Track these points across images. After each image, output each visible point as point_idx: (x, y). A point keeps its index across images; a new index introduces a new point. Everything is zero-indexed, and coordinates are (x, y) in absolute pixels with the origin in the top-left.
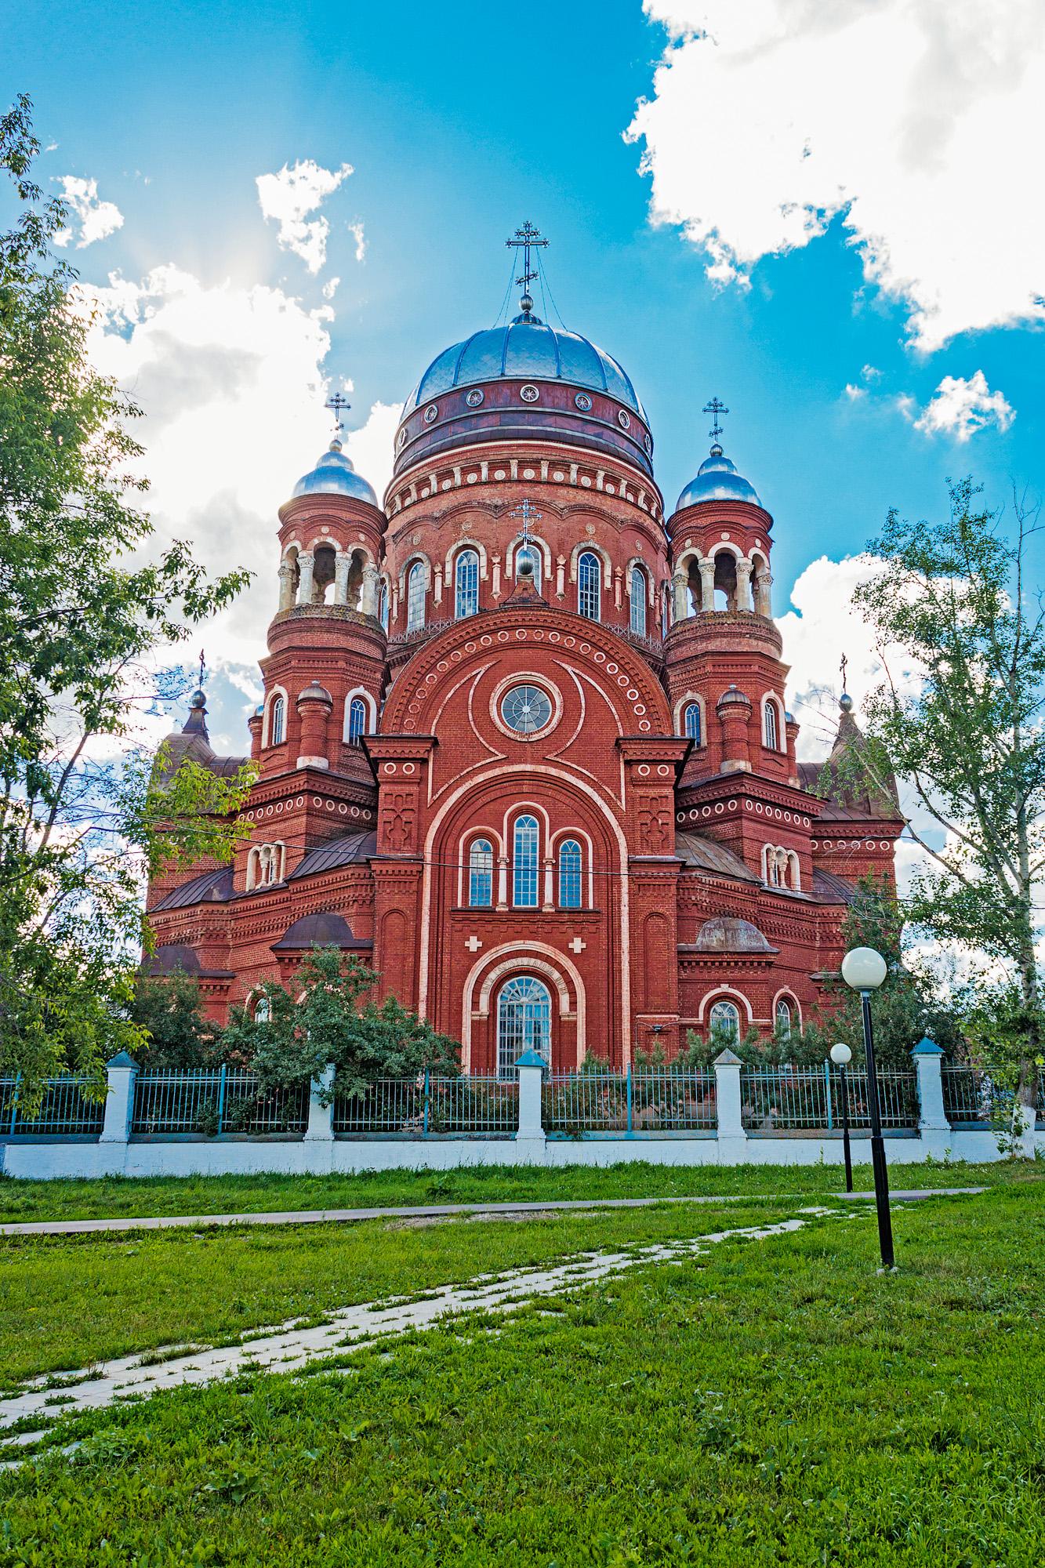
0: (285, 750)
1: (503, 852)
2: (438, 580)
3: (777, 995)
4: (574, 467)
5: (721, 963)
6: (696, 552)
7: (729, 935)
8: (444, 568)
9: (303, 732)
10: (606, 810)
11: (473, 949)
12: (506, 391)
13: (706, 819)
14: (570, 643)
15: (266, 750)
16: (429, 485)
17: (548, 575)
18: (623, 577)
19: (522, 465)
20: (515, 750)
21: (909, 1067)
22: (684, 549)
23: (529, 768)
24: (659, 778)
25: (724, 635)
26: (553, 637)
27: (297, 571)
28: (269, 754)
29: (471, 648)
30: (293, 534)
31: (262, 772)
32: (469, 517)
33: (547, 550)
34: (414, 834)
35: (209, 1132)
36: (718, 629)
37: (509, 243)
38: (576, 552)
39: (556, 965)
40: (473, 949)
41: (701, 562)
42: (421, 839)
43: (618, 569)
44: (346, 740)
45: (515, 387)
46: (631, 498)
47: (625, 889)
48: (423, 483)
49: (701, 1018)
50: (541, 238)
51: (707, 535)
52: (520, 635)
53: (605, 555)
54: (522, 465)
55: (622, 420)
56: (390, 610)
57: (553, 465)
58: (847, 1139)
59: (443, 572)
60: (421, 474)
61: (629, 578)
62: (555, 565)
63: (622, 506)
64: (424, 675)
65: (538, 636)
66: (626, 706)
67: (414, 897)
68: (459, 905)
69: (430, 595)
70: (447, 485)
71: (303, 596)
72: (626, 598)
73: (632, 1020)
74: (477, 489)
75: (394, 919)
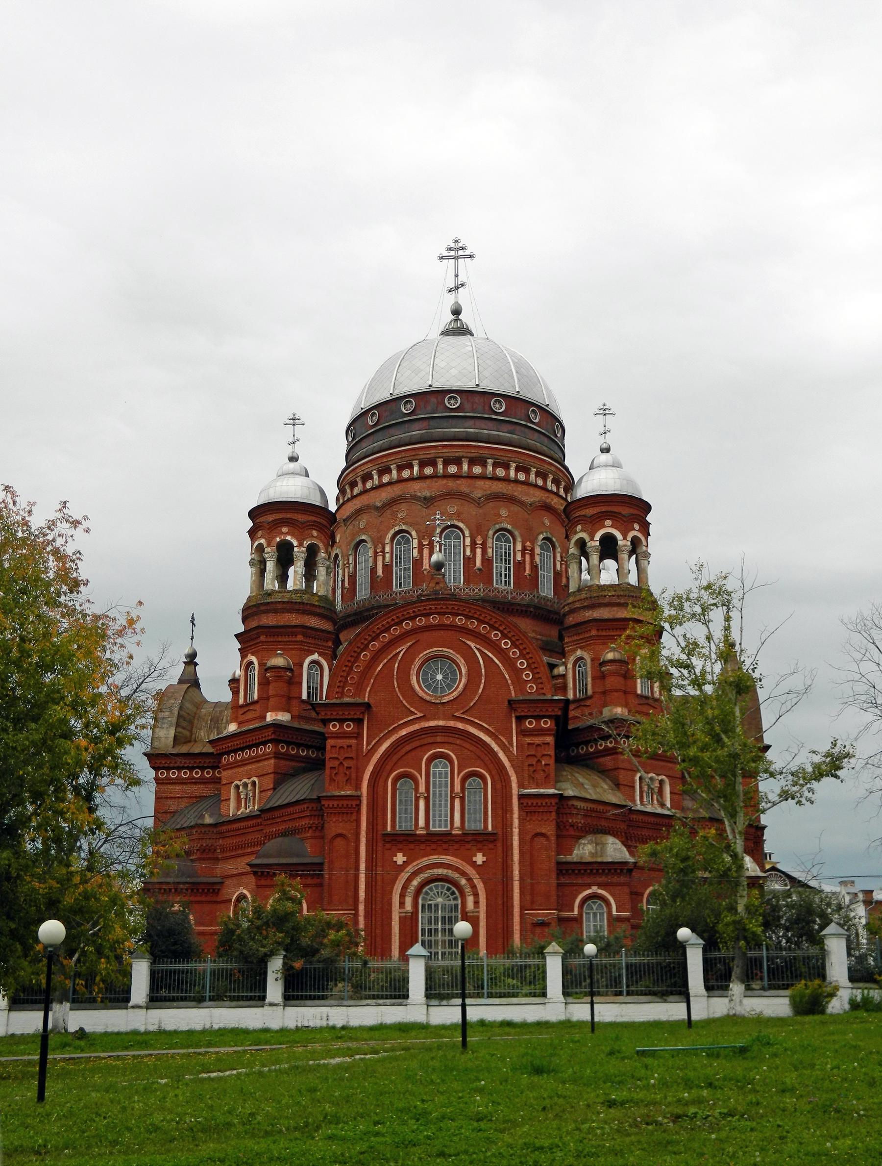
0: (257, 707)
1: (422, 789)
2: (380, 559)
3: (648, 891)
4: (490, 461)
5: (591, 870)
6: (584, 535)
7: (599, 848)
8: (384, 548)
9: (271, 692)
10: (501, 755)
11: (400, 862)
12: (433, 400)
13: (592, 753)
14: (473, 624)
15: (242, 706)
16: (372, 478)
17: (468, 553)
18: (532, 550)
19: (446, 463)
20: (431, 708)
21: (818, 941)
22: (576, 533)
23: (441, 723)
24: (543, 729)
25: (606, 605)
26: (460, 621)
27: (263, 562)
28: (245, 709)
29: (396, 631)
30: (260, 533)
31: (240, 724)
32: (404, 507)
33: (467, 533)
34: (354, 776)
35: (199, 1001)
36: (601, 601)
37: (441, 258)
38: (491, 532)
39: (463, 874)
40: (400, 862)
41: (589, 544)
42: (359, 780)
43: (528, 544)
44: (304, 696)
45: (440, 397)
46: (540, 482)
47: (516, 815)
48: (367, 477)
49: (576, 912)
50: (467, 252)
51: (595, 522)
52: (434, 620)
53: (516, 533)
54: (446, 463)
55: (532, 416)
56: (343, 581)
57: (472, 462)
58: (592, 1004)
59: (383, 551)
60: (366, 469)
61: (538, 550)
62: (473, 544)
63: (532, 491)
64: (360, 654)
65: (448, 620)
66: (516, 673)
67: (354, 824)
68: (389, 829)
69: (374, 570)
70: (386, 479)
71: (271, 583)
72: (534, 567)
73: (522, 915)
74: (411, 483)
75: (339, 842)
